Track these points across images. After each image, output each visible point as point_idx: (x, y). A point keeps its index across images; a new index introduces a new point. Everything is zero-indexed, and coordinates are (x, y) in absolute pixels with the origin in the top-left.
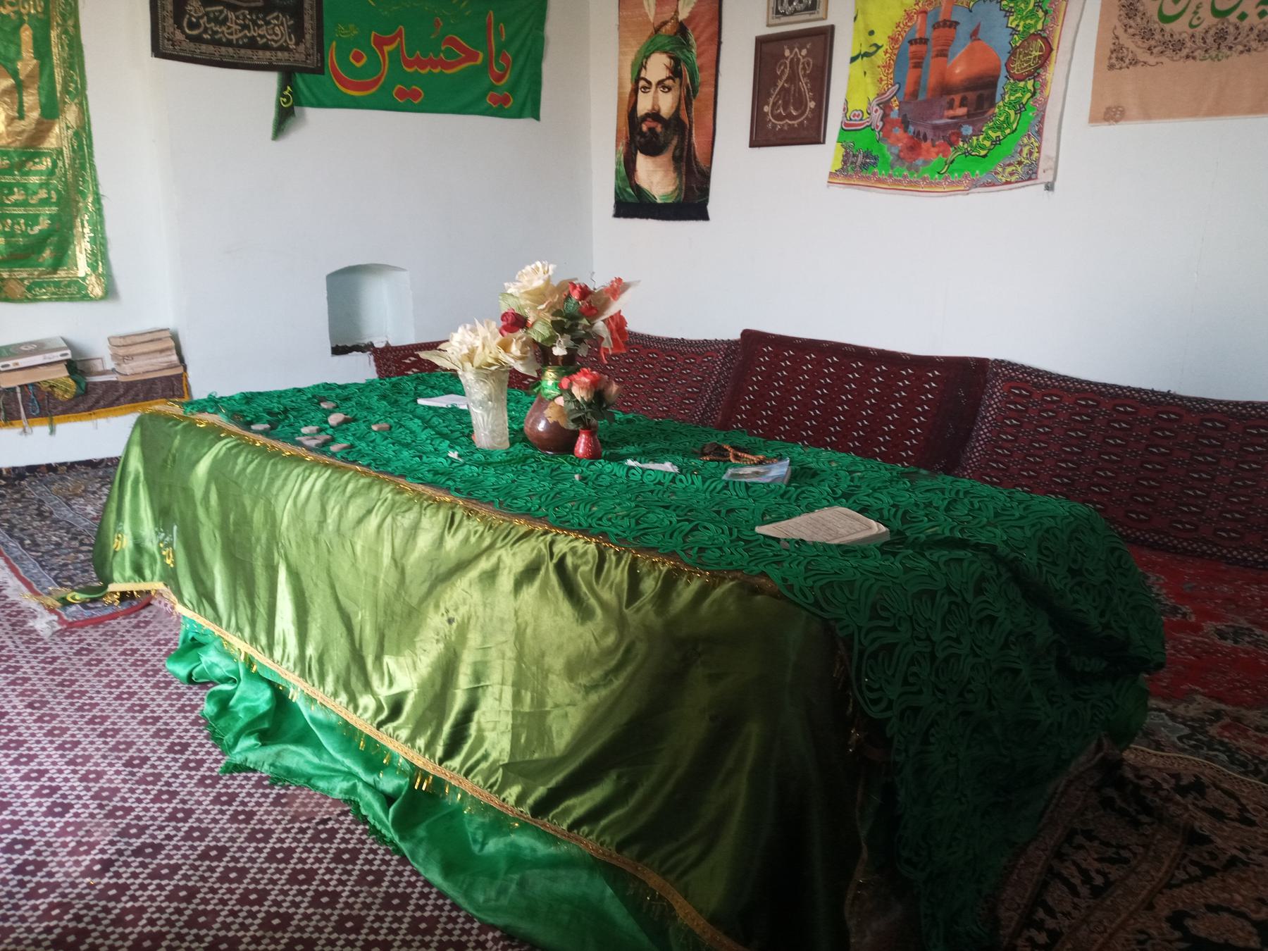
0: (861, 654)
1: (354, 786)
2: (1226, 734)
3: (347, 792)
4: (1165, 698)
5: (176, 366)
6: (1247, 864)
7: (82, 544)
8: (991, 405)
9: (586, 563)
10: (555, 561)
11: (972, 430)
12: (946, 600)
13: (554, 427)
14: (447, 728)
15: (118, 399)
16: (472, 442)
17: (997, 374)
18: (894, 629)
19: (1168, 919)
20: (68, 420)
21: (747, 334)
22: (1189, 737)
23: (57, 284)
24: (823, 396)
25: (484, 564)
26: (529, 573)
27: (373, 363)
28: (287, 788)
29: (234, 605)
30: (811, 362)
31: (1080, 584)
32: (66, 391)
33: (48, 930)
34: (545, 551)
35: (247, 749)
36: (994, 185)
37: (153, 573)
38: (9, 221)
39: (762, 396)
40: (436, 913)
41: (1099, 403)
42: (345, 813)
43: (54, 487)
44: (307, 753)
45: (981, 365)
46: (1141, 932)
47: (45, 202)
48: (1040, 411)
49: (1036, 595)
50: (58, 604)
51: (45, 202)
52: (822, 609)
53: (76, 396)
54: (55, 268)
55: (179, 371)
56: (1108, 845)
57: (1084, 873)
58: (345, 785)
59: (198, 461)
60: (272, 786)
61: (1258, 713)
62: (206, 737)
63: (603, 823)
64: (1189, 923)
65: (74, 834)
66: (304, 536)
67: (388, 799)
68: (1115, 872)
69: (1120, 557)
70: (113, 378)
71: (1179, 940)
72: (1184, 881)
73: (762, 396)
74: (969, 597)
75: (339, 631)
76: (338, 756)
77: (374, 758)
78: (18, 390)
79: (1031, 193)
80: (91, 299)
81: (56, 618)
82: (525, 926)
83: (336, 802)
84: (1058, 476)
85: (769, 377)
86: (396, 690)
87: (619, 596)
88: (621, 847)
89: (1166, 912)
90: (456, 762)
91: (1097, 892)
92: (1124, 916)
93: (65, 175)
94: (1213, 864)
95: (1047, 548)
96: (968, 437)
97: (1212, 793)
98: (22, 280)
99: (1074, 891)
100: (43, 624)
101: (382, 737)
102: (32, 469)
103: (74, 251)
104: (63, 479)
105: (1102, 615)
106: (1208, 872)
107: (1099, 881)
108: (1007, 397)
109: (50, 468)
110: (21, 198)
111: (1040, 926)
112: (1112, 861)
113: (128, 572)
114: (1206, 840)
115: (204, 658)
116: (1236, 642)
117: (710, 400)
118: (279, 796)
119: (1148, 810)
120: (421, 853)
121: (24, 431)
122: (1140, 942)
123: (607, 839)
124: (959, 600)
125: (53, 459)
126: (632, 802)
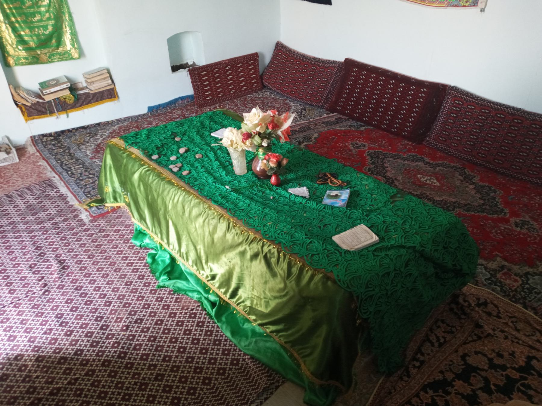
0: (361, 300)
1: (201, 298)
2: (503, 277)
3: (199, 298)
4: (486, 259)
5: (111, 85)
6: (492, 336)
7: (90, 174)
8: (446, 106)
9: (274, 257)
10: (264, 254)
11: (437, 116)
12: (393, 274)
13: (263, 171)
14: (231, 290)
15: (90, 101)
16: (234, 174)
17: (450, 93)
18: (374, 290)
19: (461, 357)
20: (73, 111)
21: (347, 60)
22: (489, 279)
23: (60, 54)
24: (377, 94)
25: (241, 249)
26: (255, 256)
27: (189, 75)
28: (179, 295)
29: (153, 225)
30: (373, 77)
31: (447, 251)
32: (70, 100)
33: (115, 352)
34: (260, 249)
35: (163, 280)
36: (458, 6)
37: (121, 200)
38: (36, 30)
39: (352, 91)
40: (230, 347)
41: (490, 112)
42: (199, 306)
43: (73, 139)
44: (184, 283)
45: (444, 87)
46: (451, 361)
47: (49, 19)
48: (466, 112)
49: (428, 259)
50: (88, 207)
51: (49, 19)
52: (350, 289)
53: (74, 101)
54: (58, 47)
55: (112, 86)
56: (448, 325)
57: (438, 338)
58: (198, 296)
59: (134, 173)
60: (174, 294)
61: (517, 267)
62: (150, 272)
63: (280, 334)
64: (467, 358)
65: (114, 314)
66: (177, 213)
67: (213, 304)
68: (448, 337)
69: (465, 236)
70: (87, 91)
71: (462, 365)
72: (471, 341)
73: (352, 91)
74: (402, 270)
75: (192, 247)
76: (195, 286)
77: (207, 290)
78: (52, 101)
79: (474, 11)
80: (74, 59)
81: (88, 213)
82: (257, 356)
83: (195, 302)
84: (469, 141)
85: (356, 82)
86: (213, 273)
87: (284, 272)
88: (286, 342)
89: (461, 354)
90: (234, 300)
91: (441, 345)
92: (447, 355)
93: (55, 6)
94: (482, 335)
95: (436, 241)
96: (435, 119)
97: (490, 306)
98: (46, 54)
99: (433, 345)
100: (84, 216)
101: (209, 284)
102: (63, 132)
103: (64, 40)
104: (75, 135)
105: (453, 261)
106: (479, 338)
107: (442, 340)
108: (453, 104)
109: (69, 131)
110: (39, 18)
111: (417, 360)
112: (448, 332)
113: (112, 200)
114: (481, 327)
115: (145, 241)
116: (521, 228)
117: (330, 90)
118: (177, 299)
119: (465, 314)
120: (224, 327)
121: (57, 117)
122: (450, 365)
123: (282, 339)
124: (399, 272)
125: (70, 127)
126: (290, 332)
